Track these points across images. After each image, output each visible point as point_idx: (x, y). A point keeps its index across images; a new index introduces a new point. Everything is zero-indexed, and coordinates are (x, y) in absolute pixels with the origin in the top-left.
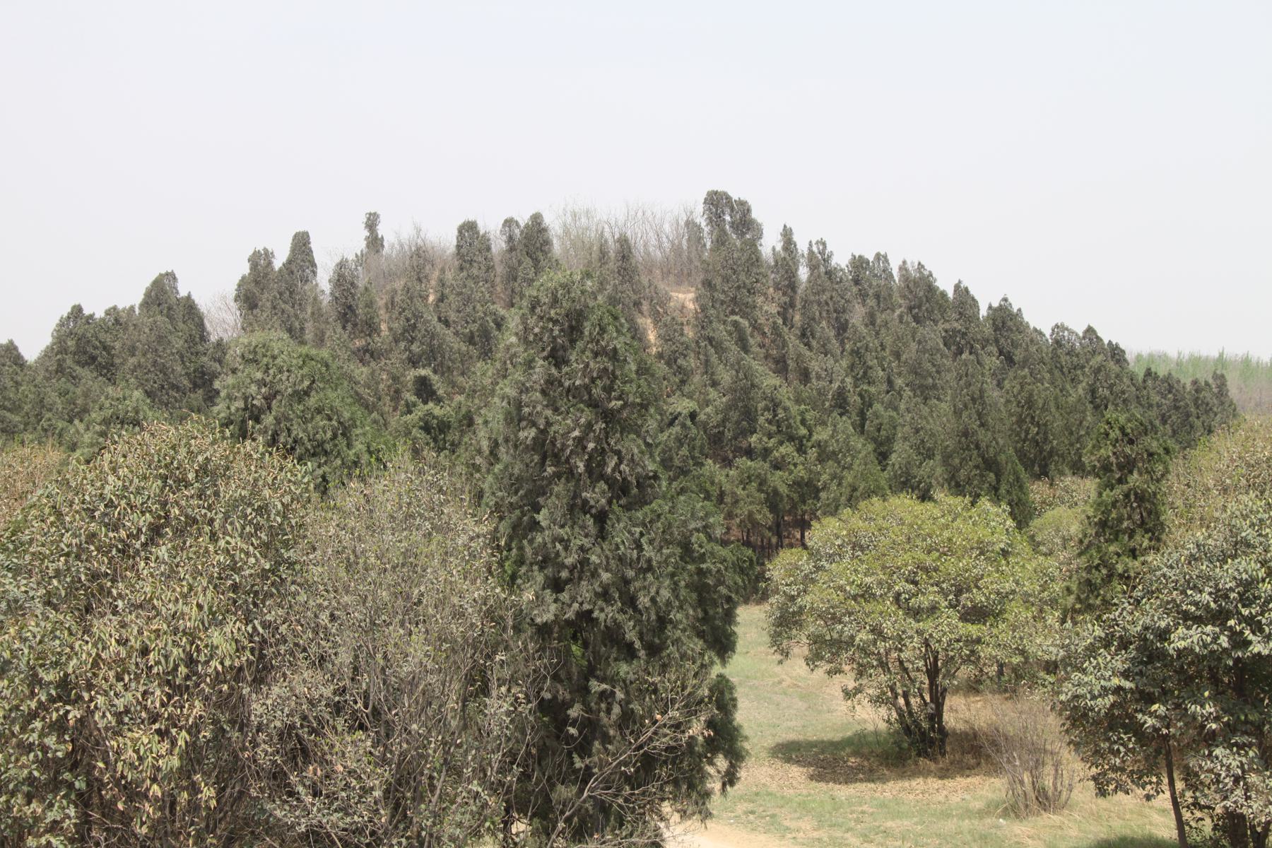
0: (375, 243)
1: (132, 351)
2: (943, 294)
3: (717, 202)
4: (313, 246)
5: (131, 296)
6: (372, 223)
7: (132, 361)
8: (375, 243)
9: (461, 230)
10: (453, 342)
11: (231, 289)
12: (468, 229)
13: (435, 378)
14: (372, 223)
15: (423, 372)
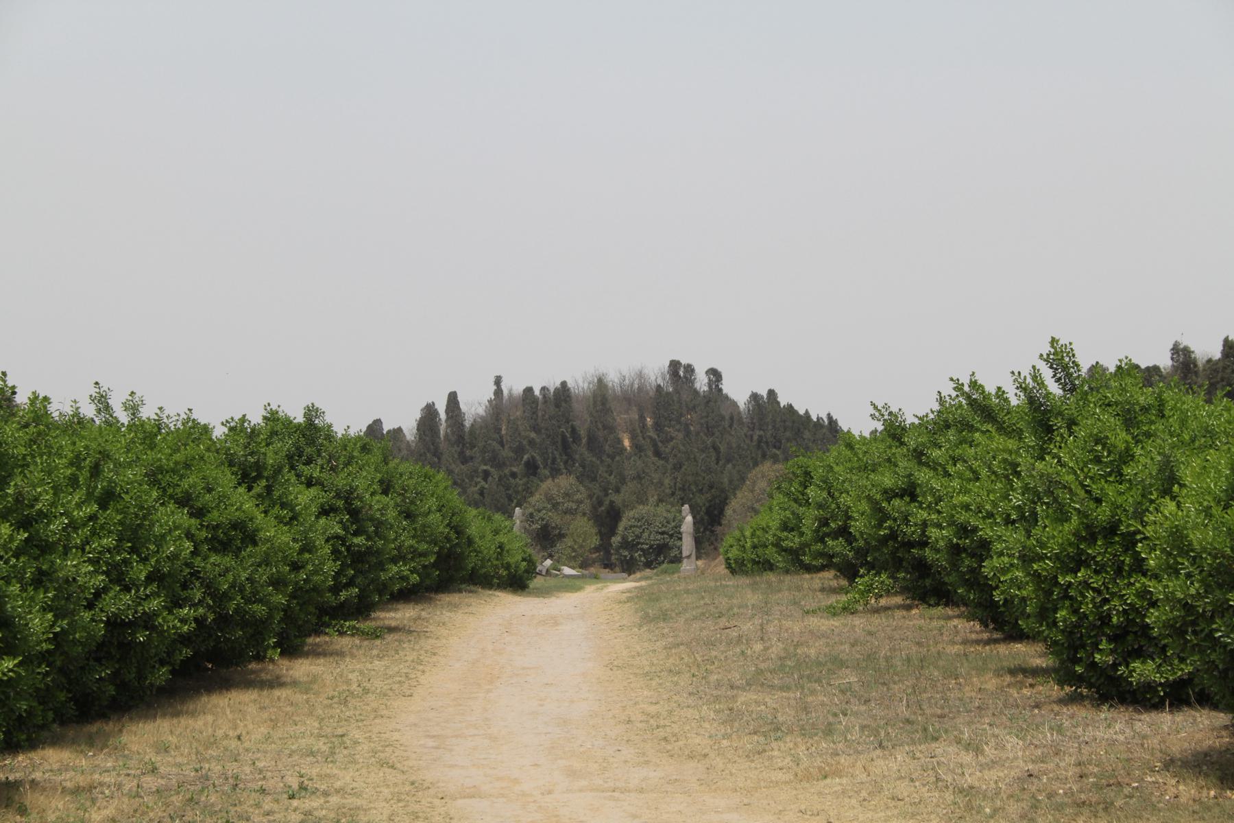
3: (675, 365)
6: (498, 381)
8: (498, 392)
11: (415, 424)
12: (529, 390)
14: (498, 381)
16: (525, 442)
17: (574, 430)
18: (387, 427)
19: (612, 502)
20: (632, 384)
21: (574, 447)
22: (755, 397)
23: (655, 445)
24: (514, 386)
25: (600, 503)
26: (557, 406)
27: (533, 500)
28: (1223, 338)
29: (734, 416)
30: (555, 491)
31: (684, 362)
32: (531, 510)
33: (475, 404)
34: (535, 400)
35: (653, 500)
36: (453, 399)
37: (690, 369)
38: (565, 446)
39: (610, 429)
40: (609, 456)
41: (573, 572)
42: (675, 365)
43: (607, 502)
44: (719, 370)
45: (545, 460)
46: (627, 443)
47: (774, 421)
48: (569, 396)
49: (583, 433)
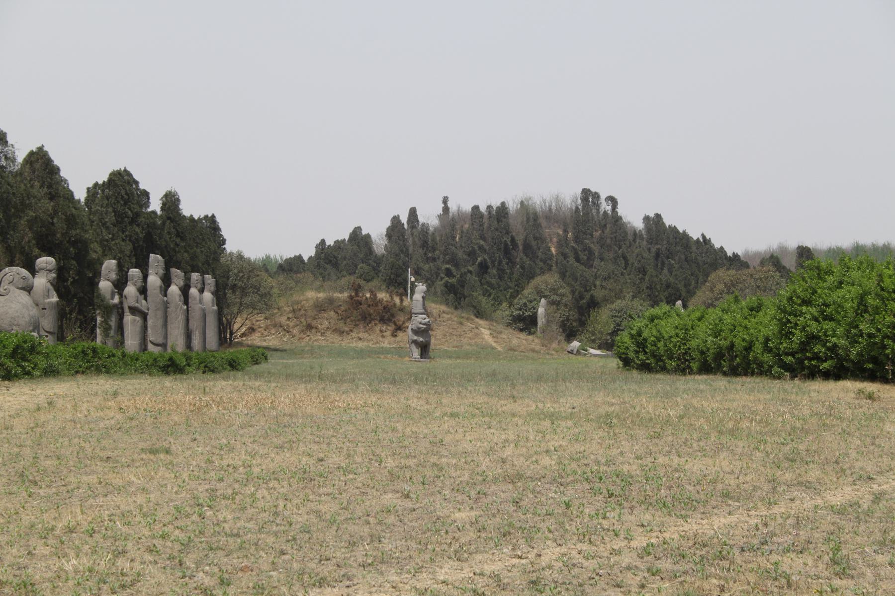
0: (446, 209)
1: (345, 258)
2: (79, 201)
3: (586, 192)
4: (418, 213)
5: (344, 235)
6: (445, 201)
7: (345, 262)
8: (446, 209)
9: (473, 208)
10: (461, 254)
11: (384, 231)
12: (476, 208)
13: (453, 269)
14: (445, 201)
15: (447, 266)
16: (476, 247)
17: (513, 240)
18: (364, 232)
19: (592, 296)
20: (550, 206)
21: (514, 253)
22: (647, 219)
23: (576, 253)
24: (462, 203)
25: (582, 298)
26: (499, 221)
27: (526, 292)
28: (39, 145)
29: (636, 234)
30: (543, 287)
31: (593, 190)
32: (524, 301)
33: (429, 216)
34: (481, 216)
35: (629, 296)
36: (413, 213)
37: (596, 196)
38: (507, 252)
39: (540, 239)
40: (541, 261)
41: (598, 352)
42: (586, 192)
43: (588, 296)
44: (616, 197)
45: (493, 262)
46: (553, 250)
47: (668, 238)
48: (507, 214)
49: (520, 240)
